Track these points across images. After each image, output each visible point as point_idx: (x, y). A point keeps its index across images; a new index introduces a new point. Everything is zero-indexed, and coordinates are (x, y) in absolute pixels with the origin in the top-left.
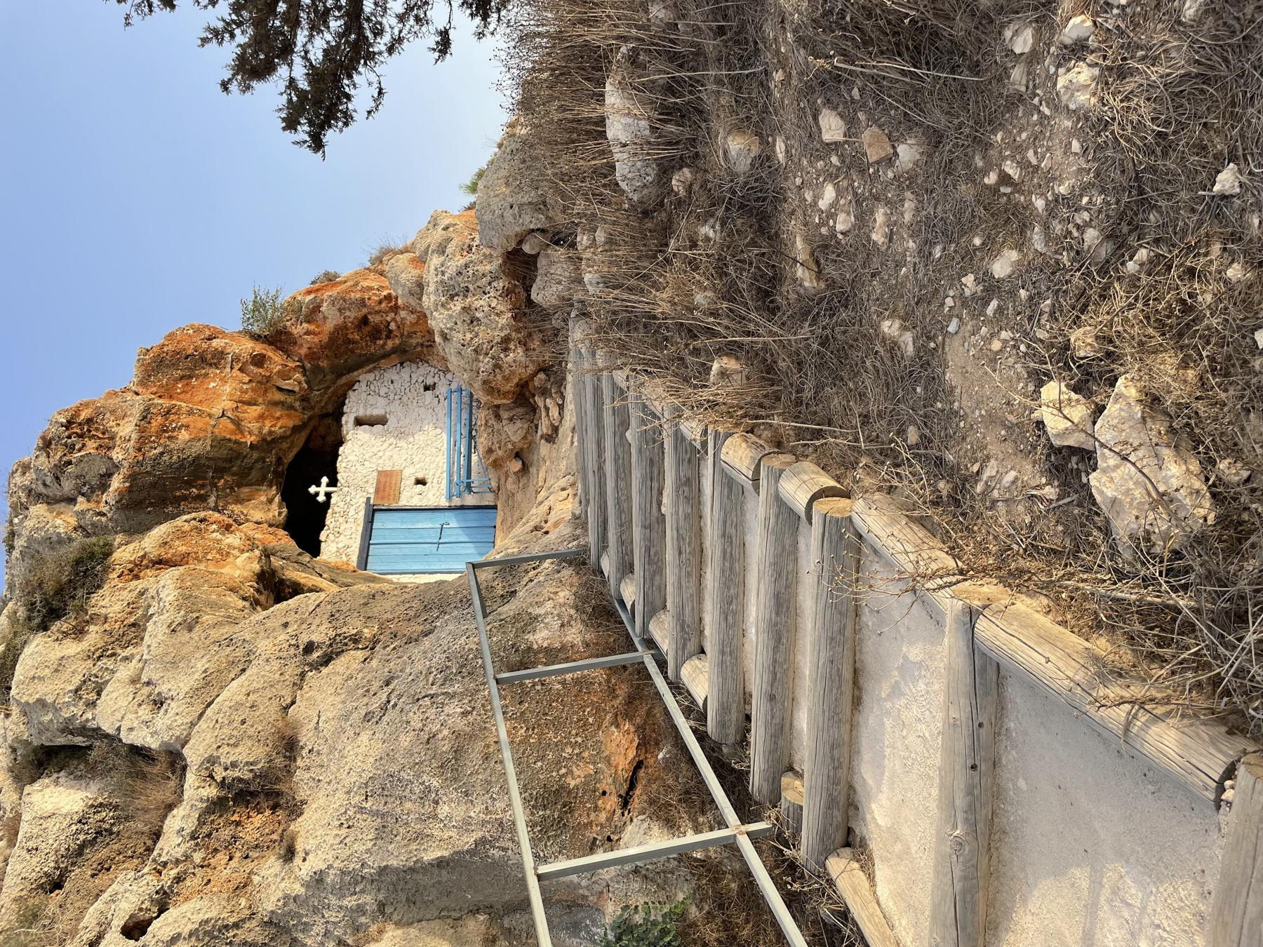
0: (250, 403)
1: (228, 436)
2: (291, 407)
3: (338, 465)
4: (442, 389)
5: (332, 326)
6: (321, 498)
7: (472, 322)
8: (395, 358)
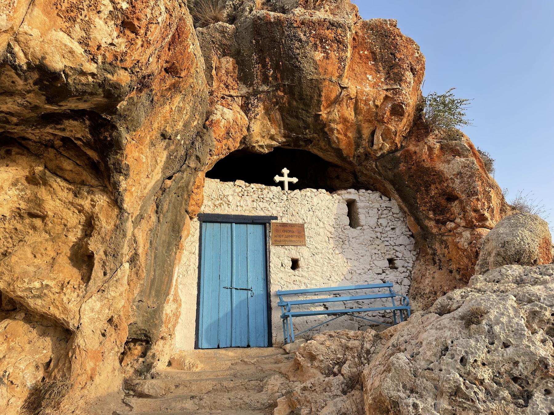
1: (323, 94)
2: (358, 145)
3: (308, 189)
4: (391, 276)
5: (442, 168)
7: (515, 379)
8: (416, 230)
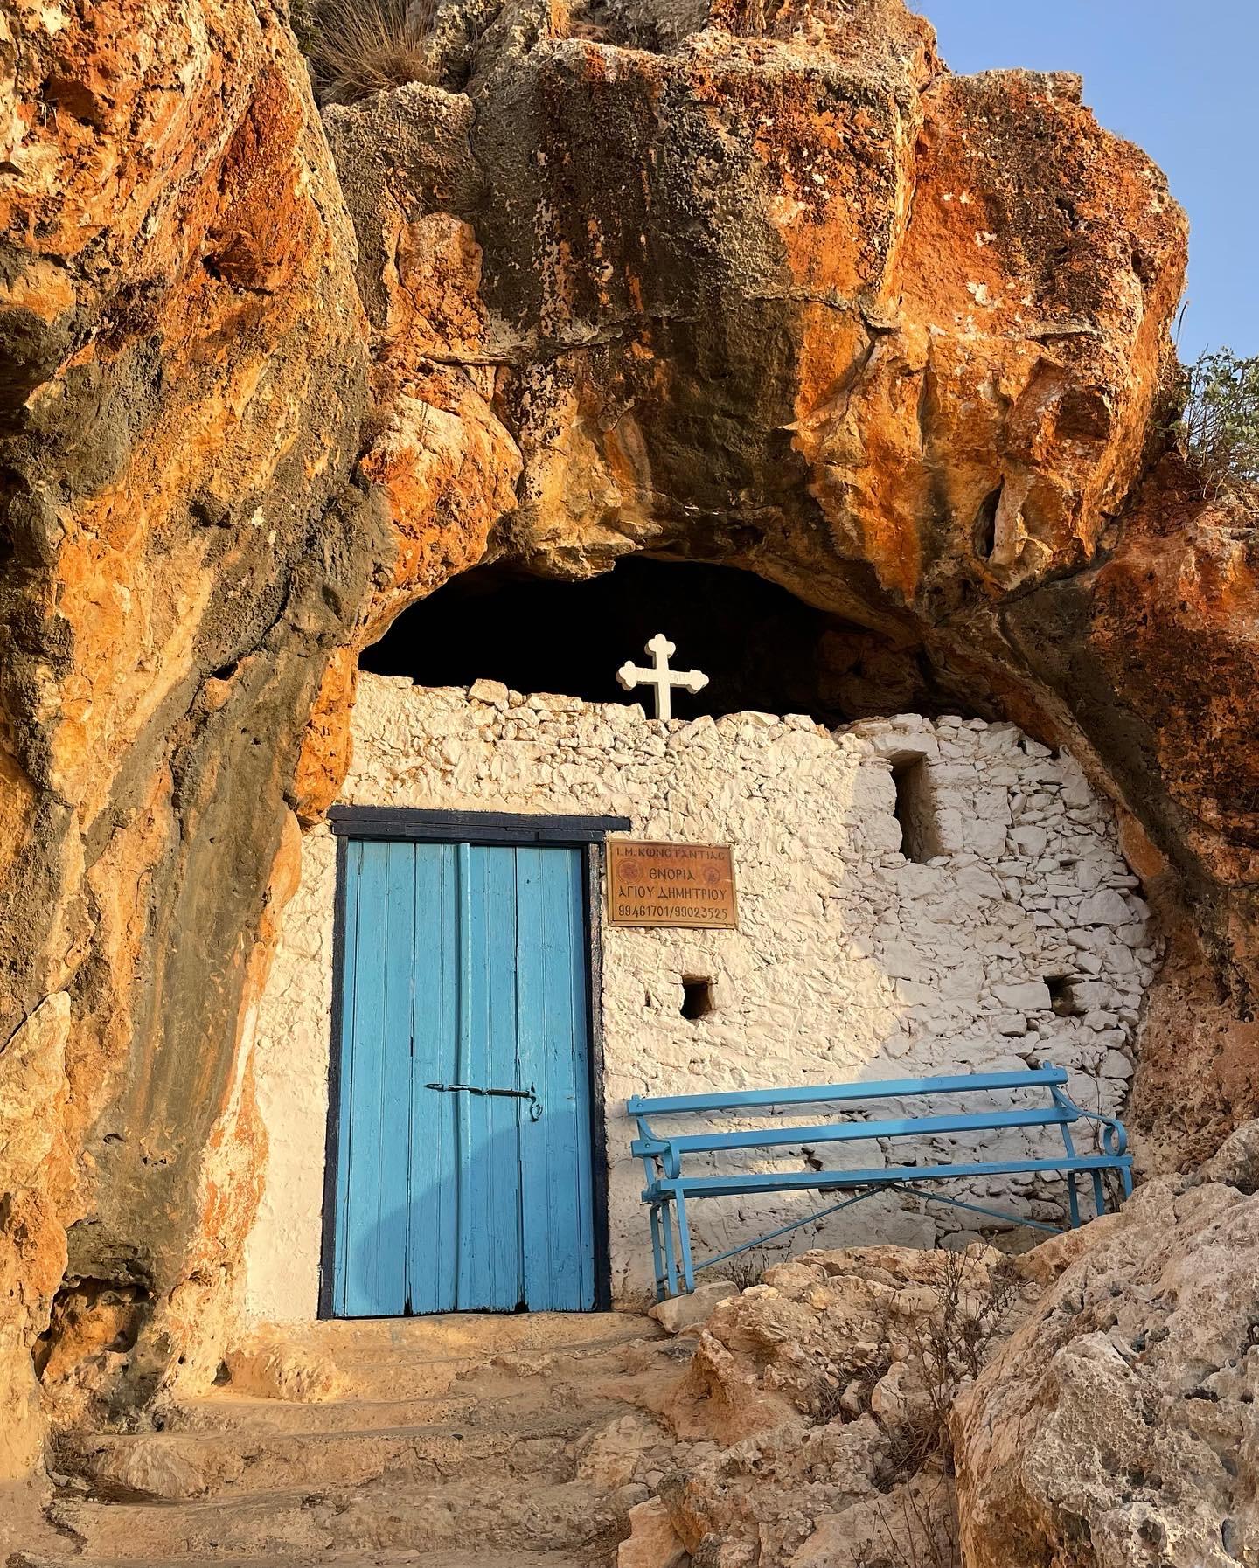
0: (928, 413)
1: (803, 355)
2: (934, 549)
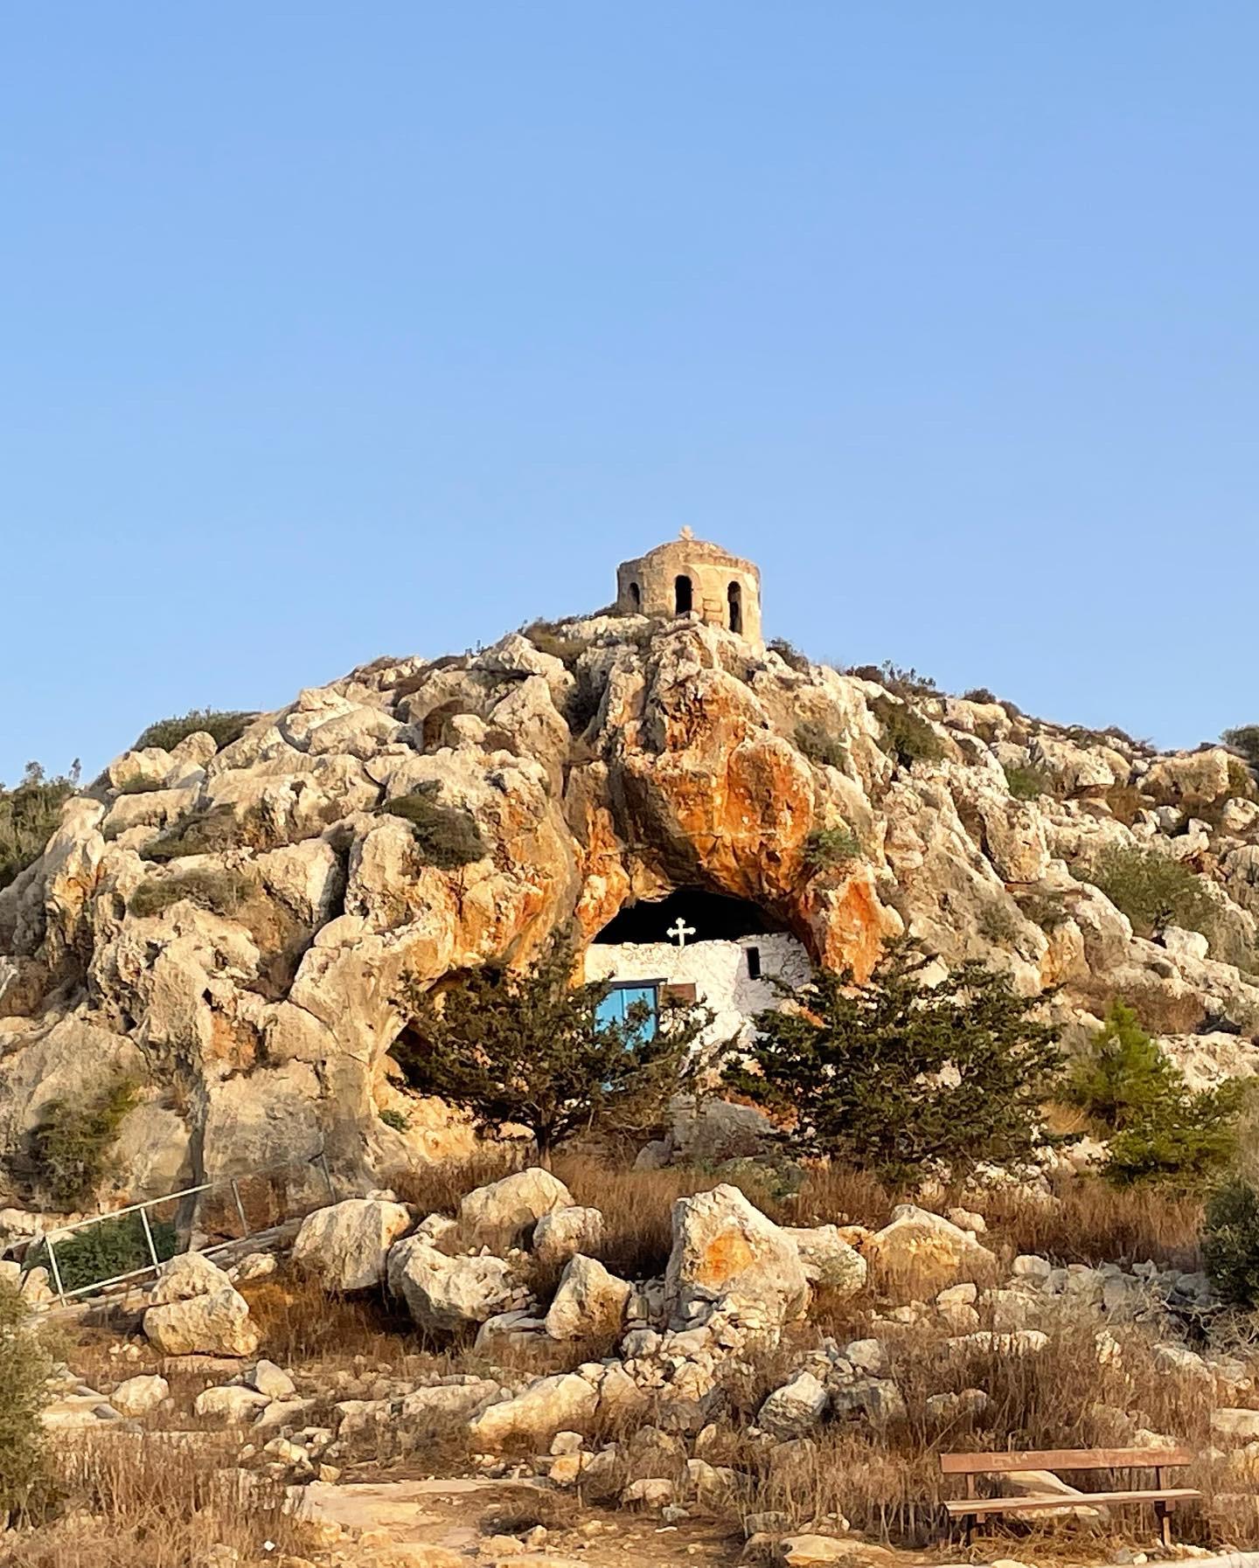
6: (671, 932)
